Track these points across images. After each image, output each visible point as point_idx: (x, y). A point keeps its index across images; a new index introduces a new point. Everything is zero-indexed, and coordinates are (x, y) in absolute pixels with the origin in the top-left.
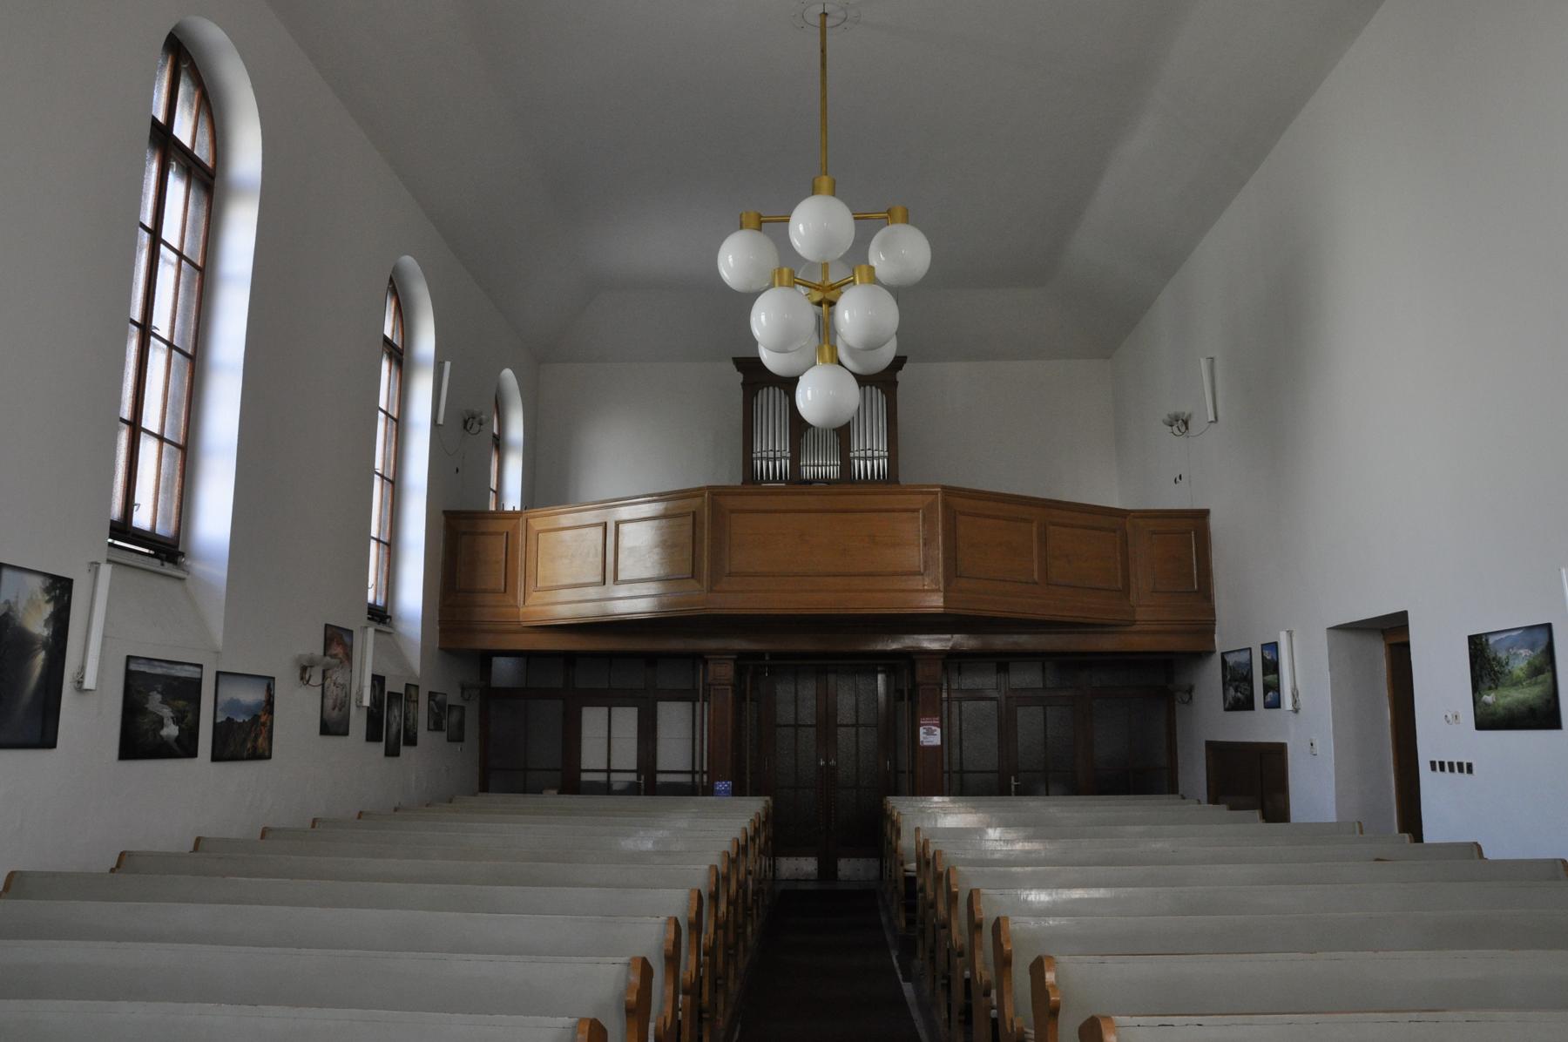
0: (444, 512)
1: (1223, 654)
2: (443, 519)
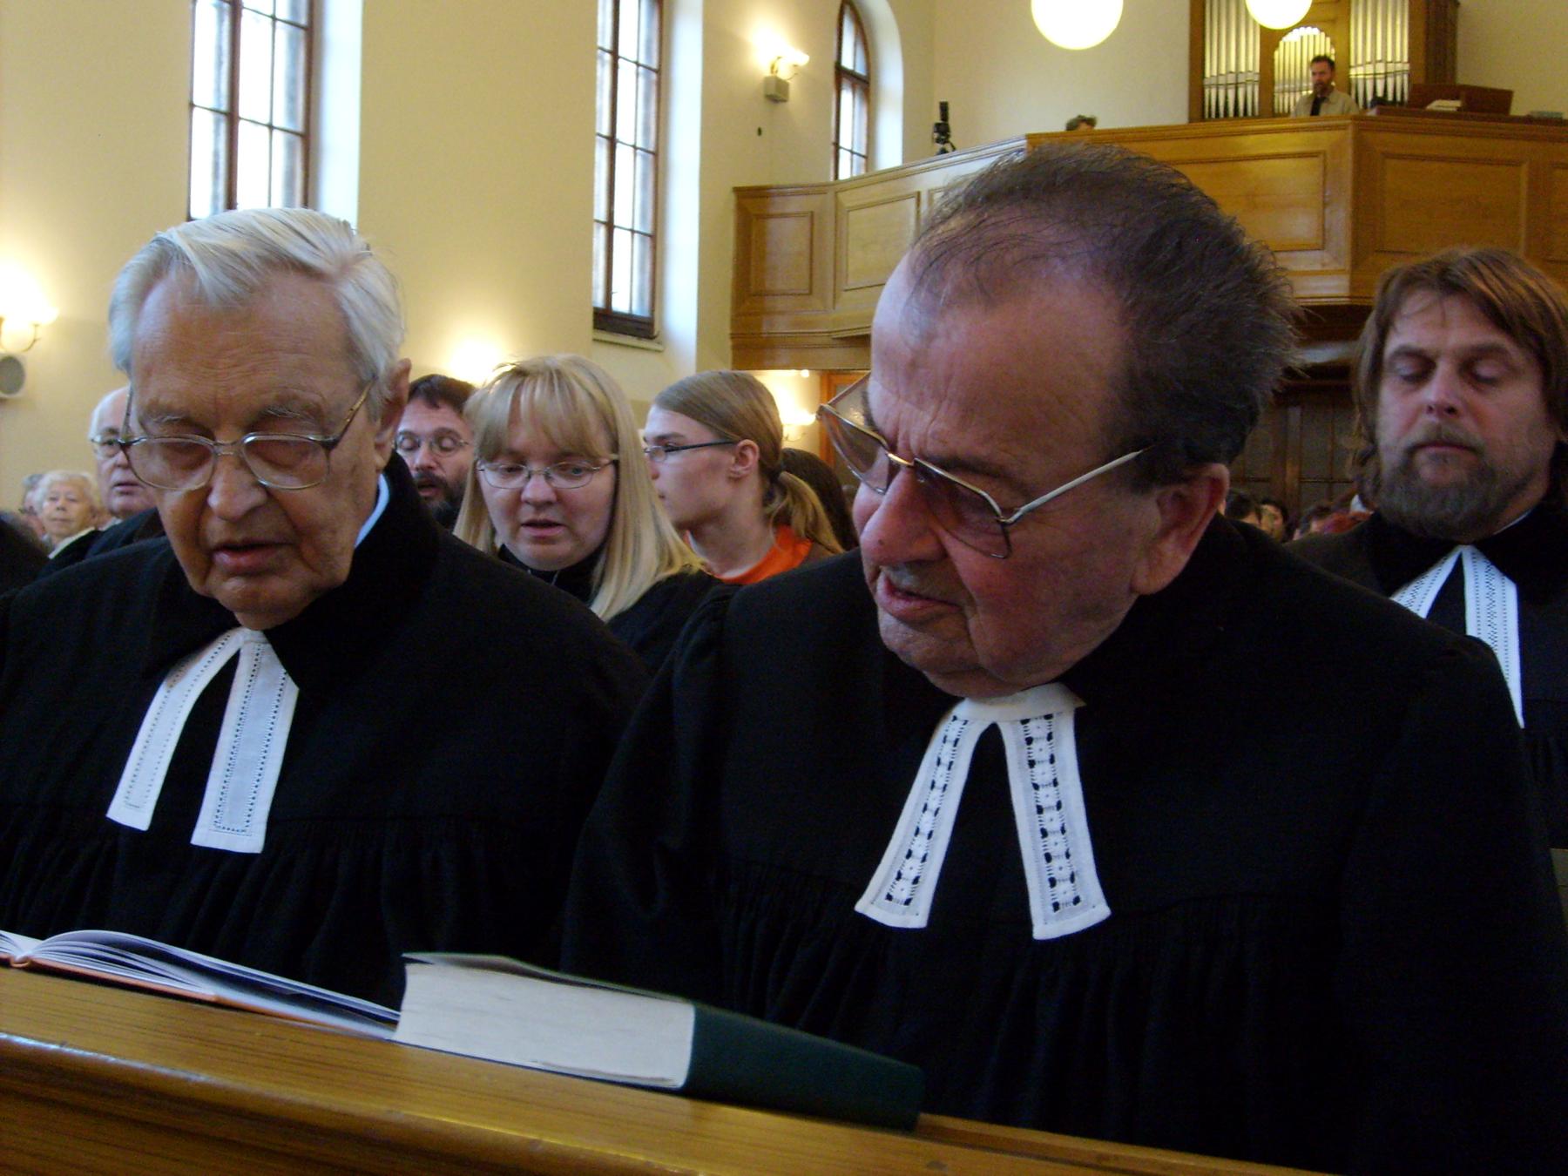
0: (737, 190)
1: (884, 494)
2: (732, 198)
